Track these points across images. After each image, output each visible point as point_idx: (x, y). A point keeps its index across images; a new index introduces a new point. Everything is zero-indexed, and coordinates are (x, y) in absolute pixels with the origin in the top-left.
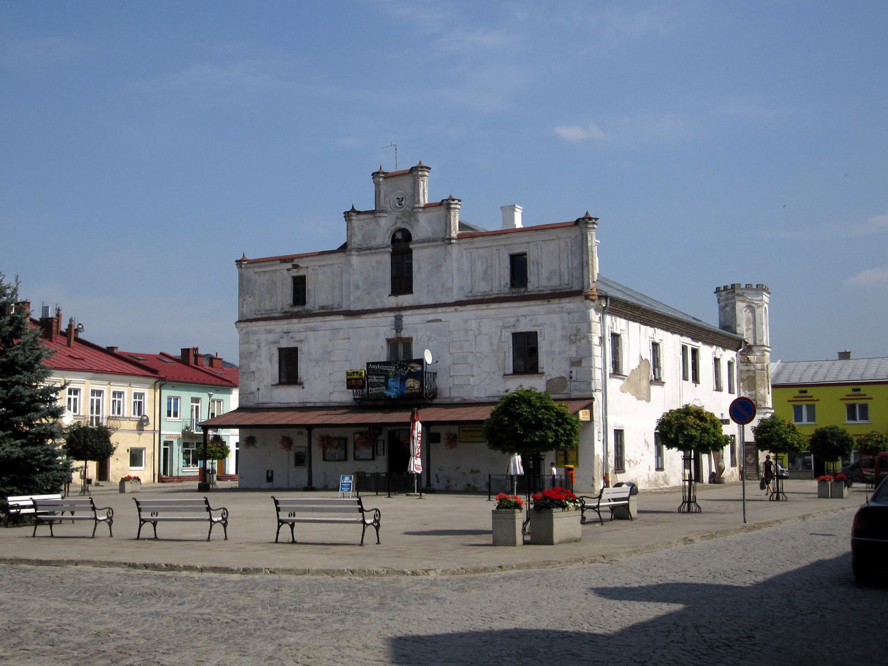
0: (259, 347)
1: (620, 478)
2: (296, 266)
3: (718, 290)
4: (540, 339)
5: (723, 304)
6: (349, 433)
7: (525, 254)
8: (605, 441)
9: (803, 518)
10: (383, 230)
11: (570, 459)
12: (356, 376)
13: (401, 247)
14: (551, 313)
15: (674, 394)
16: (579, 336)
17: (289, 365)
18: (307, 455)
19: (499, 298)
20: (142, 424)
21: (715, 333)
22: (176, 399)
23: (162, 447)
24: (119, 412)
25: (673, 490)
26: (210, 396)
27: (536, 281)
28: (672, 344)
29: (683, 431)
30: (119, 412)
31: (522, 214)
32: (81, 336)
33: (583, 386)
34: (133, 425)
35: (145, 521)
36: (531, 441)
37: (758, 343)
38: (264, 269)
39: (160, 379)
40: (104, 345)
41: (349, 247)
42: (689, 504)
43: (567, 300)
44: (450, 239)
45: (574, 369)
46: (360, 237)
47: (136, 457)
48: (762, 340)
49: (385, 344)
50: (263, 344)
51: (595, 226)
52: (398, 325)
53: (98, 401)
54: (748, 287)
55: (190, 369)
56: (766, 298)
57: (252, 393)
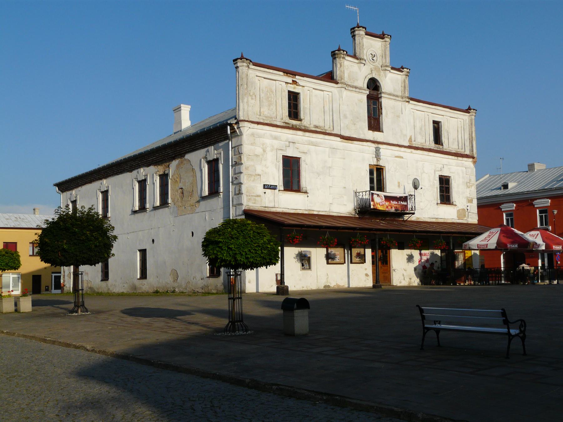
0: (264, 151)
3: (328, 263)
50: (268, 149)
52: (378, 156)
57: (258, 196)
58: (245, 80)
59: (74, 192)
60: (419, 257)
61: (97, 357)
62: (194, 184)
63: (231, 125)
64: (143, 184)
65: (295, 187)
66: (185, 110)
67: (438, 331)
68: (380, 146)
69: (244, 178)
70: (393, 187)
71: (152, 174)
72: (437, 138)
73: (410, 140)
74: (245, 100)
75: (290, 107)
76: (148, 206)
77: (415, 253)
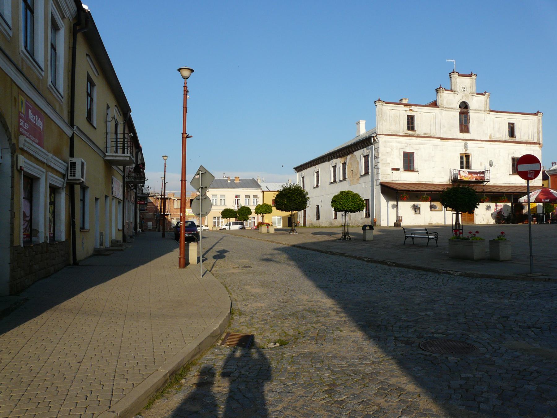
27: (519, 136)
52: (466, 147)
58: (380, 112)
59: (303, 172)
60: (495, 207)
61: (284, 246)
62: (358, 168)
63: (373, 137)
64: (334, 167)
65: (412, 169)
66: (362, 124)
67: (413, 238)
68: (468, 142)
69: (380, 165)
70: (476, 167)
71: (338, 162)
72: (512, 133)
73: (490, 136)
74: (381, 123)
75: (408, 123)
76: (337, 180)
77: (492, 205)
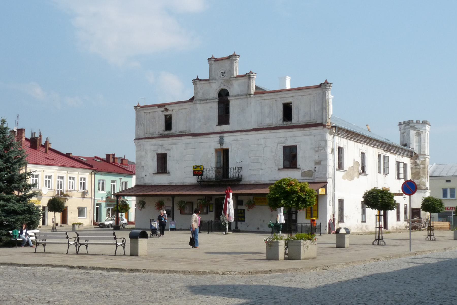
1: (341, 225)
2: (166, 110)
4: (298, 150)
5: (402, 131)
6: (194, 200)
7: (291, 103)
8: (333, 206)
9: (445, 249)
10: (213, 91)
11: (314, 215)
12: (198, 169)
13: (223, 97)
14: (305, 135)
15: (374, 180)
16: (321, 148)
17: (162, 162)
18: (171, 212)
19: (280, 127)
20: (84, 194)
21: (398, 148)
22: (103, 181)
23: (96, 206)
24: (72, 188)
25: (371, 233)
26: (120, 179)
27: (297, 118)
28: (372, 153)
29: (378, 200)
30: (72, 188)
31: (290, 81)
32: (52, 147)
33: (322, 175)
34: (80, 194)
35: (81, 244)
36: (293, 205)
37: (422, 153)
38: (149, 111)
39: (95, 170)
40: (65, 152)
41: (195, 99)
42: (379, 239)
43: (314, 128)
44: (250, 95)
45: (317, 166)
46: (201, 93)
47: (81, 211)
48: (424, 152)
49: (214, 152)
50: (148, 151)
51: (330, 87)
52: (221, 142)
53: (61, 182)
54: (418, 122)
55: (110, 165)
56: (428, 128)
72: (168, 125)
